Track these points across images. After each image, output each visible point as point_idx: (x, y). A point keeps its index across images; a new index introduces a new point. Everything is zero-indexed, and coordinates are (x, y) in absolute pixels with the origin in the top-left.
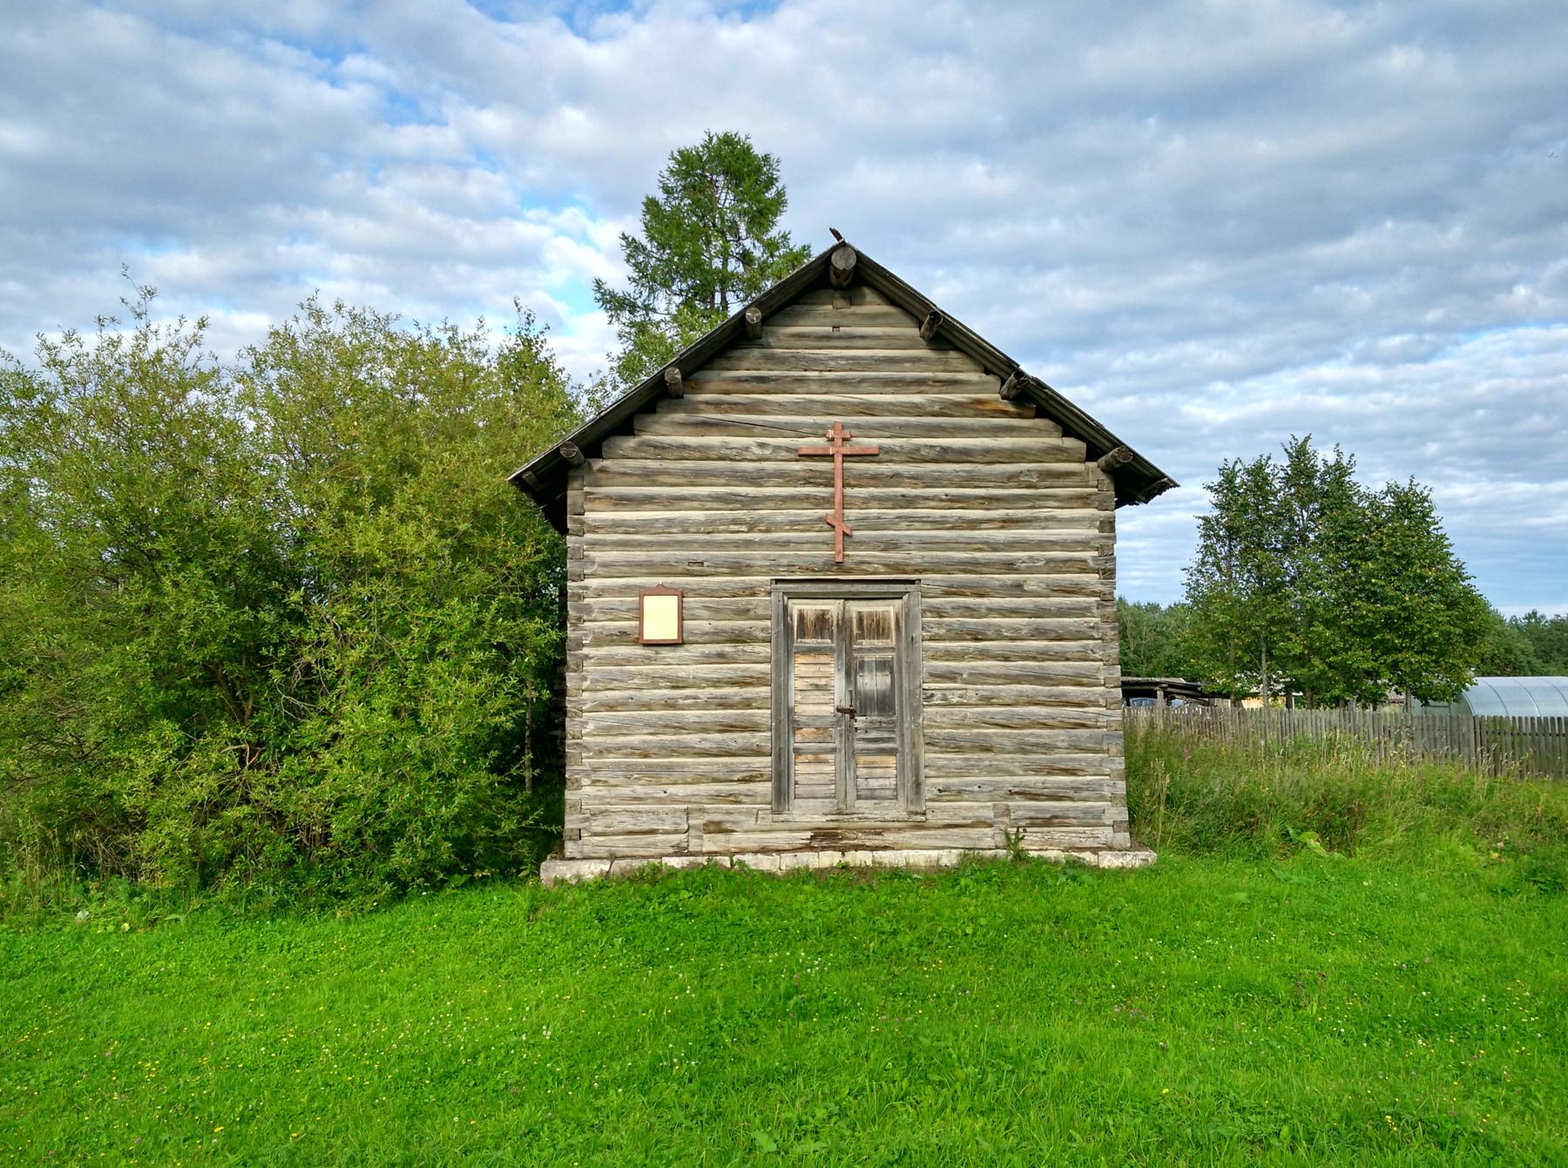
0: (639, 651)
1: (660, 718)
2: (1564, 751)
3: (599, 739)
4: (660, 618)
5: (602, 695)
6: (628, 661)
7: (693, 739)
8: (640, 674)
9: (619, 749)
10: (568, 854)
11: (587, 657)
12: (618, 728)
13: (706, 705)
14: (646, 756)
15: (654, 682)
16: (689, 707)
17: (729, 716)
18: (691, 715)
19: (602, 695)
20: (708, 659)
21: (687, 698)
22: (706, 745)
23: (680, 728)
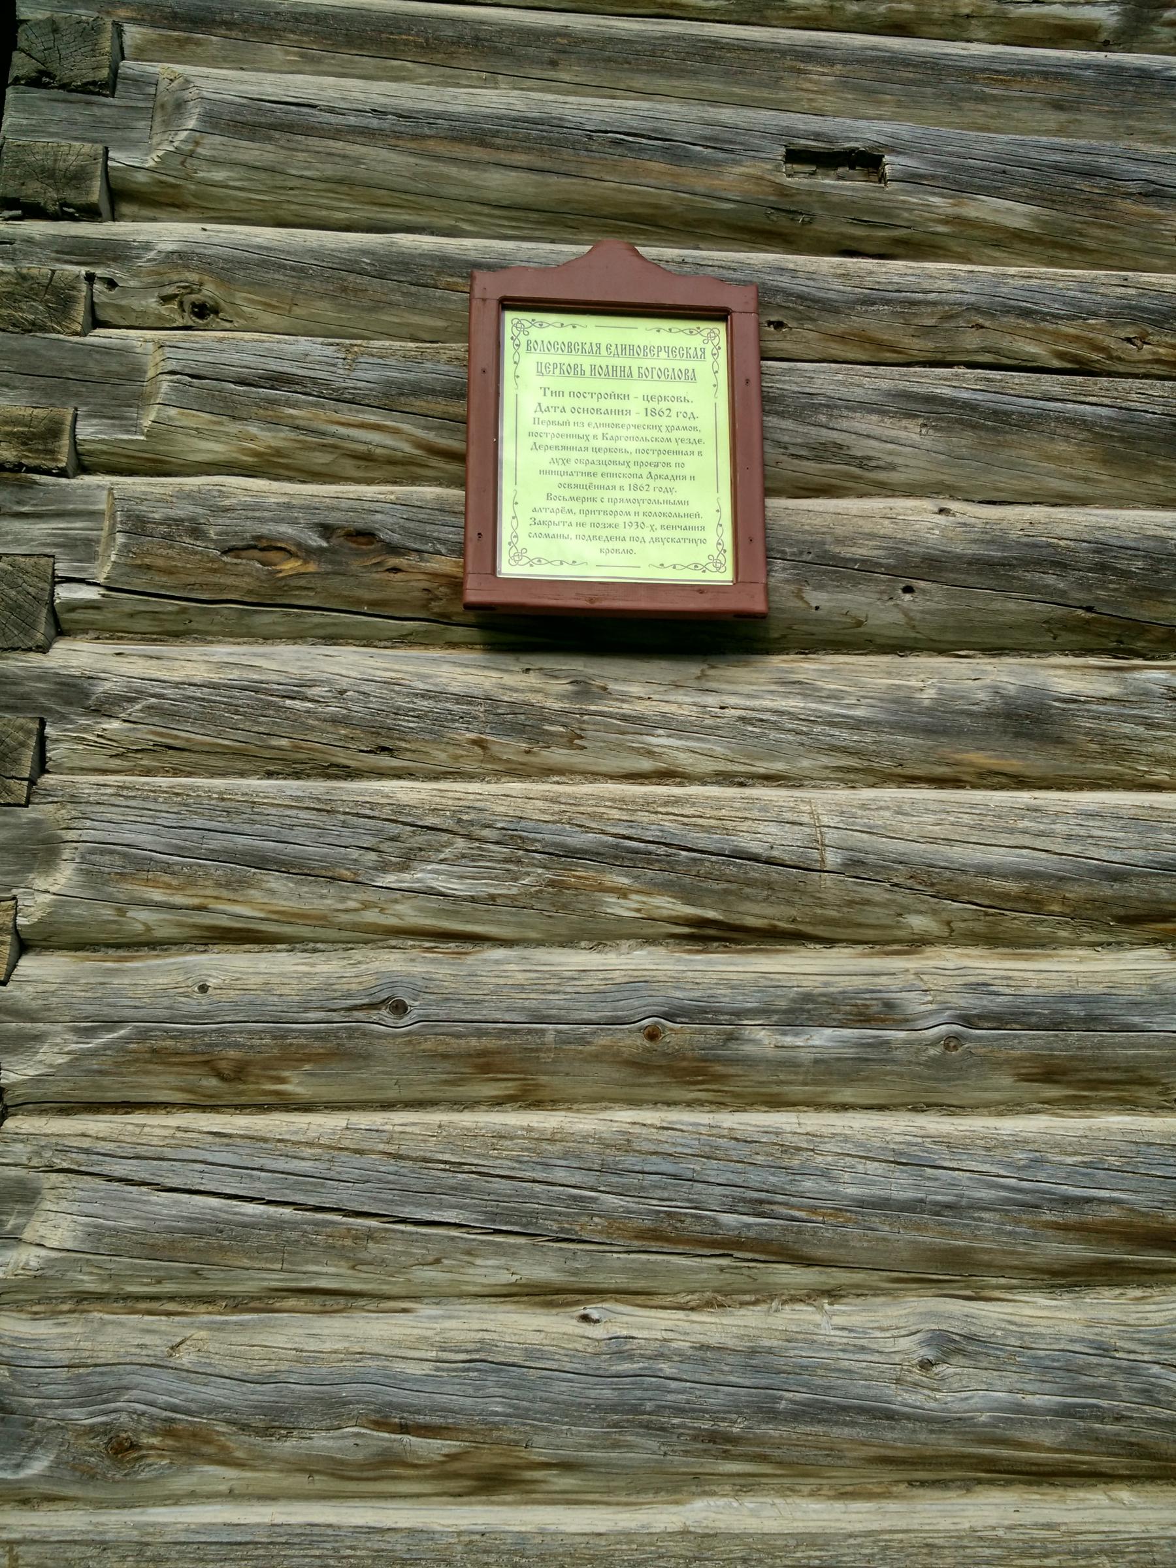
0: (460, 673)
1: (609, 1163)
2: (1073, 1564)
3: (119, 1337)
4: (613, 450)
5: (156, 981)
6: (384, 739)
7: (874, 1333)
8: (466, 826)
9: (276, 1421)
10: (753, 289)
11: (75, 693)
12: (279, 1243)
13: (937, 1078)
14: (492, 1483)
15: (562, 887)
16: (819, 1086)
17: (1136, 1158)
18: (849, 1142)
19: (156, 981)
20: (930, 747)
21: (803, 1011)
22: (972, 1392)
23: (771, 1242)
